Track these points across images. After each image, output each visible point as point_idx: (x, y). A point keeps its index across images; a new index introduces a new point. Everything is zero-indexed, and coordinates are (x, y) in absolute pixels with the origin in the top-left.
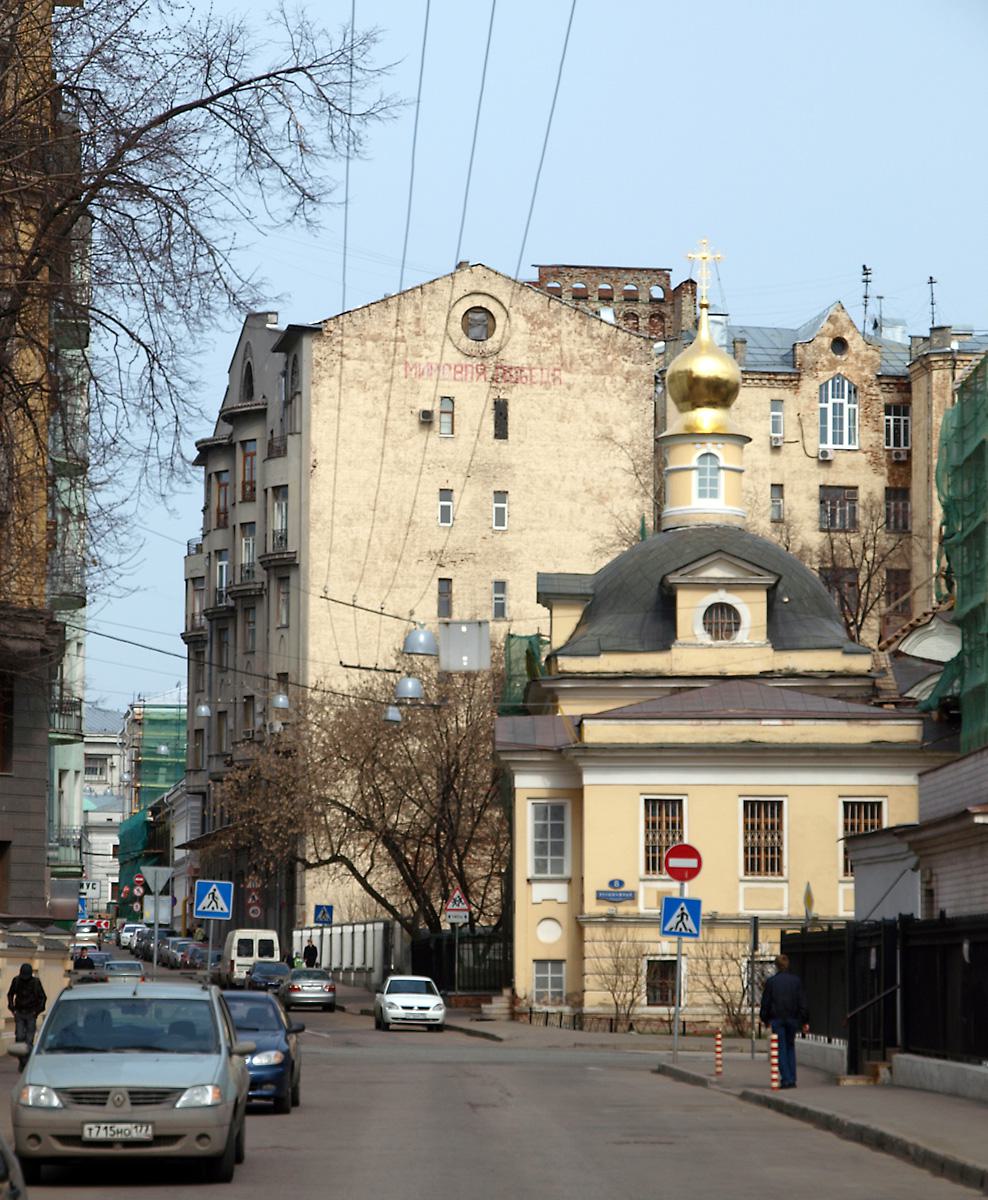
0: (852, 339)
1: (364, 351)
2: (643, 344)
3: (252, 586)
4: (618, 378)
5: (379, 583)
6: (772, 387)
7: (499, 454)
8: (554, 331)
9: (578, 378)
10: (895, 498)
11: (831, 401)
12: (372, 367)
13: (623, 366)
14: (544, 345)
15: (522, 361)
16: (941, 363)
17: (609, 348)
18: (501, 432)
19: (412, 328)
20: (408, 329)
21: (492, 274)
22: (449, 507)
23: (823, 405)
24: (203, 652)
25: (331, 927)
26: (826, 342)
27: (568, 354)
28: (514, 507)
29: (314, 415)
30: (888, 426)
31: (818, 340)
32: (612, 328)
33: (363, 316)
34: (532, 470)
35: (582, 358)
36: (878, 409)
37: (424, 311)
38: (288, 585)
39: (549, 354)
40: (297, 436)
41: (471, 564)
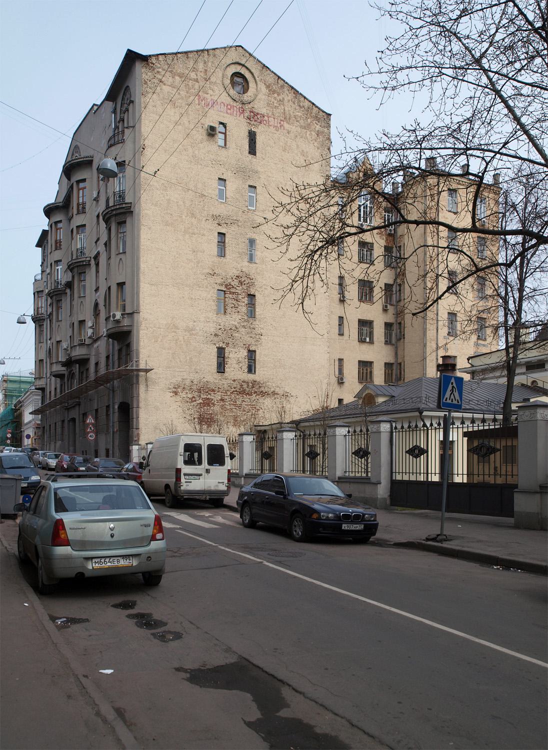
4: (313, 133)
8: (280, 97)
9: (294, 128)
15: (263, 111)
18: (252, 151)
32: (310, 103)
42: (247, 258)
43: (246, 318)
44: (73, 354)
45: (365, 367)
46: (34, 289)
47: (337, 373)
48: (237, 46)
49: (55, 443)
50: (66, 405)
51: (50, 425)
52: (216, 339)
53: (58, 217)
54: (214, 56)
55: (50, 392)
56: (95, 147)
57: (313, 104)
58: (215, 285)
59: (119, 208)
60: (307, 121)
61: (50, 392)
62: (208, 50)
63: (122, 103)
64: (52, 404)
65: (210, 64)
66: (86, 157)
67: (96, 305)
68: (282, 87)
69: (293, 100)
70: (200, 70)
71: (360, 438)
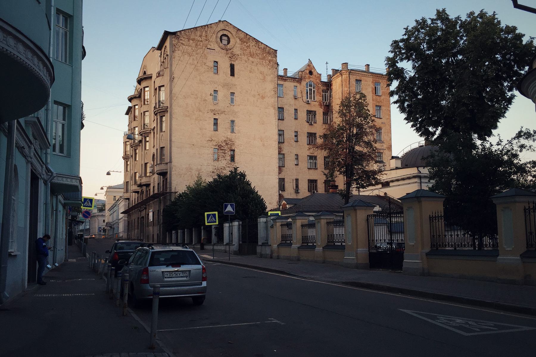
0: (314, 71)
3: (148, 130)
4: (267, 61)
7: (232, 81)
8: (248, 44)
9: (256, 60)
10: (325, 115)
11: (309, 88)
12: (192, 49)
13: (268, 58)
15: (239, 53)
18: (232, 74)
20: (204, 38)
22: (217, 96)
23: (307, 89)
25: (267, 217)
26: (308, 72)
28: (237, 98)
31: (306, 71)
32: (265, 46)
33: (189, 32)
34: (242, 87)
35: (256, 54)
36: (320, 91)
37: (208, 33)
41: (224, 115)
42: (229, 131)
43: (230, 162)
44: (142, 181)
45: (312, 183)
46: (124, 140)
47: (295, 187)
48: (223, 21)
49: (135, 230)
50: (140, 209)
51: (132, 220)
52: (213, 174)
53: (135, 102)
54: (211, 27)
55: (132, 201)
56: (153, 70)
57: (267, 46)
58: (212, 146)
59: (162, 109)
60: (263, 55)
61: (132, 201)
62: (207, 25)
63: (164, 53)
64: (134, 208)
65: (208, 32)
66: (149, 75)
67: (154, 155)
68: (249, 39)
69: (255, 45)
70: (203, 36)
71: (379, 220)
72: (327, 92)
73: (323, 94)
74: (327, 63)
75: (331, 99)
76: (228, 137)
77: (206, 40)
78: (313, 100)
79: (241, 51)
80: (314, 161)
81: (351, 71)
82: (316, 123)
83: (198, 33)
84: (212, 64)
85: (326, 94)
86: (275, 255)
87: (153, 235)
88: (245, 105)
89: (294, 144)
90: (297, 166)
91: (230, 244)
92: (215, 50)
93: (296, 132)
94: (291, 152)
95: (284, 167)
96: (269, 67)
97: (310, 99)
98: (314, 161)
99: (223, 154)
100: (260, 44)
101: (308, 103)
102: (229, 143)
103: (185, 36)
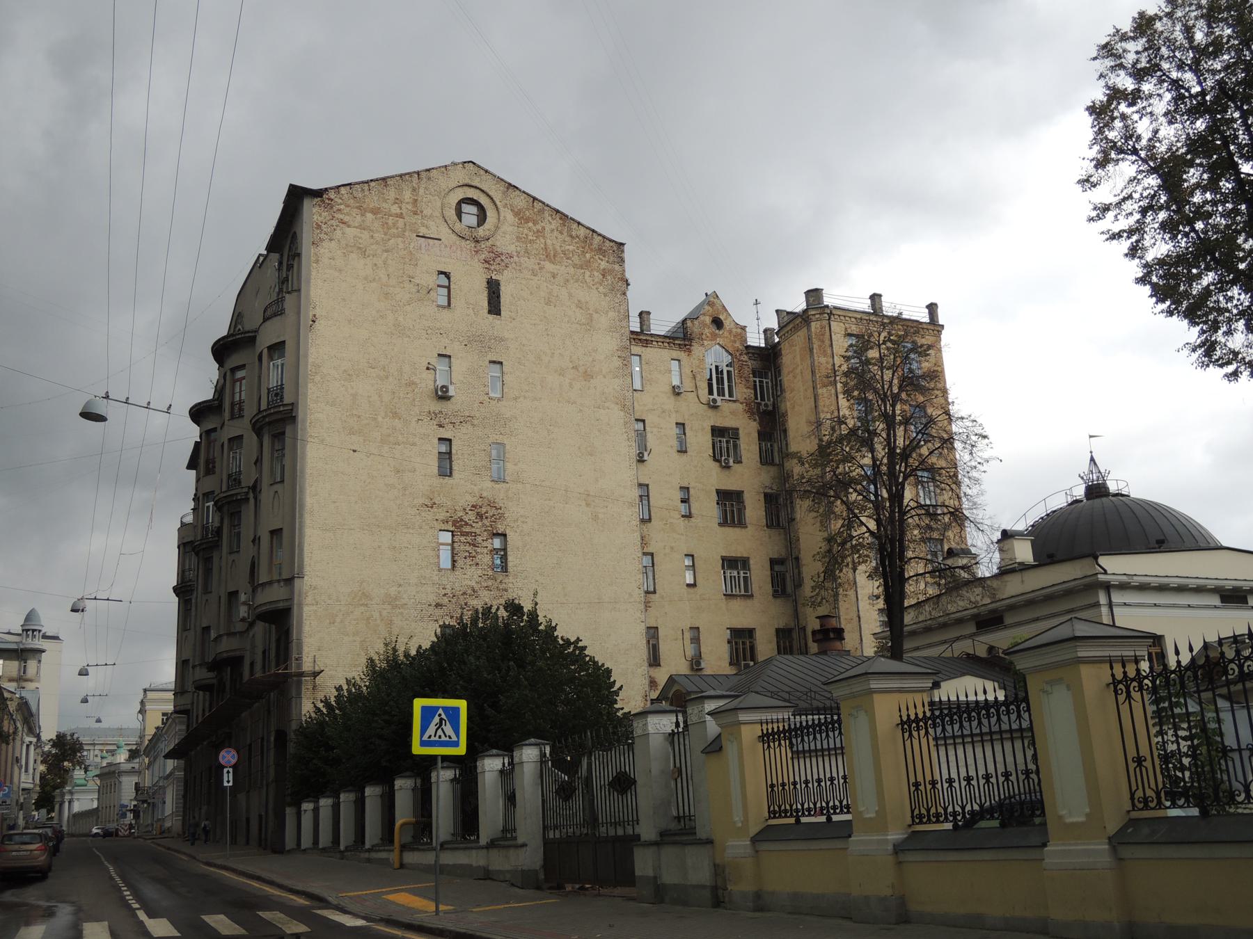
0: (725, 319)
1: (363, 221)
2: (615, 248)
4: (596, 274)
5: (379, 439)
6: (671, 348)
9: (563, 270)
14: (530, 238)
15: (512, 249)
16: (817, 316)
17: (587, 247)
18: (494, 307)
19: (410, 207)
20: (407, 207)
21: (482, 172)
24: (191, 599)
26: (708, 320)
27: (551, 247)
29: (314, 273)
30: (755, 385)
31: (702, 318)
32: (588, 231)
36: (747, 371)
38: (284, 440)
39: (535, 246)
40: (295, 294)
41: (470, 427)
52: (439, 612)
57: (593, 231)
58: (435, 522)
62: (418, 173)
68: (541, 211)
72: (766, 374)
73: (755, 382)
74: (757, 303)
75: (779, 393)
76: (485, 494)
77: (415, 213)
78: (727, 396)
79: (517, 244)
80: (742, 572)
81: (834, 312)
82: (740, 462)
83: (392, 194)
84: (432, 280)
85: (765, 380)
86: (741, 887)
87: (248, 820)
88: (535, 399)
89: (682, 523)
90: (691, 590)
91: (506, 839)
92: (440, 240)
93: (685, 489)
94: (672, 548)
95: (654, 592)
96: (601, 289)
97: (719, 395)
98: (742, 572)
99: (468, 548)
100: (575, 226)
101: (713, 406)
102: (487, 512)
103: (352, 201)
